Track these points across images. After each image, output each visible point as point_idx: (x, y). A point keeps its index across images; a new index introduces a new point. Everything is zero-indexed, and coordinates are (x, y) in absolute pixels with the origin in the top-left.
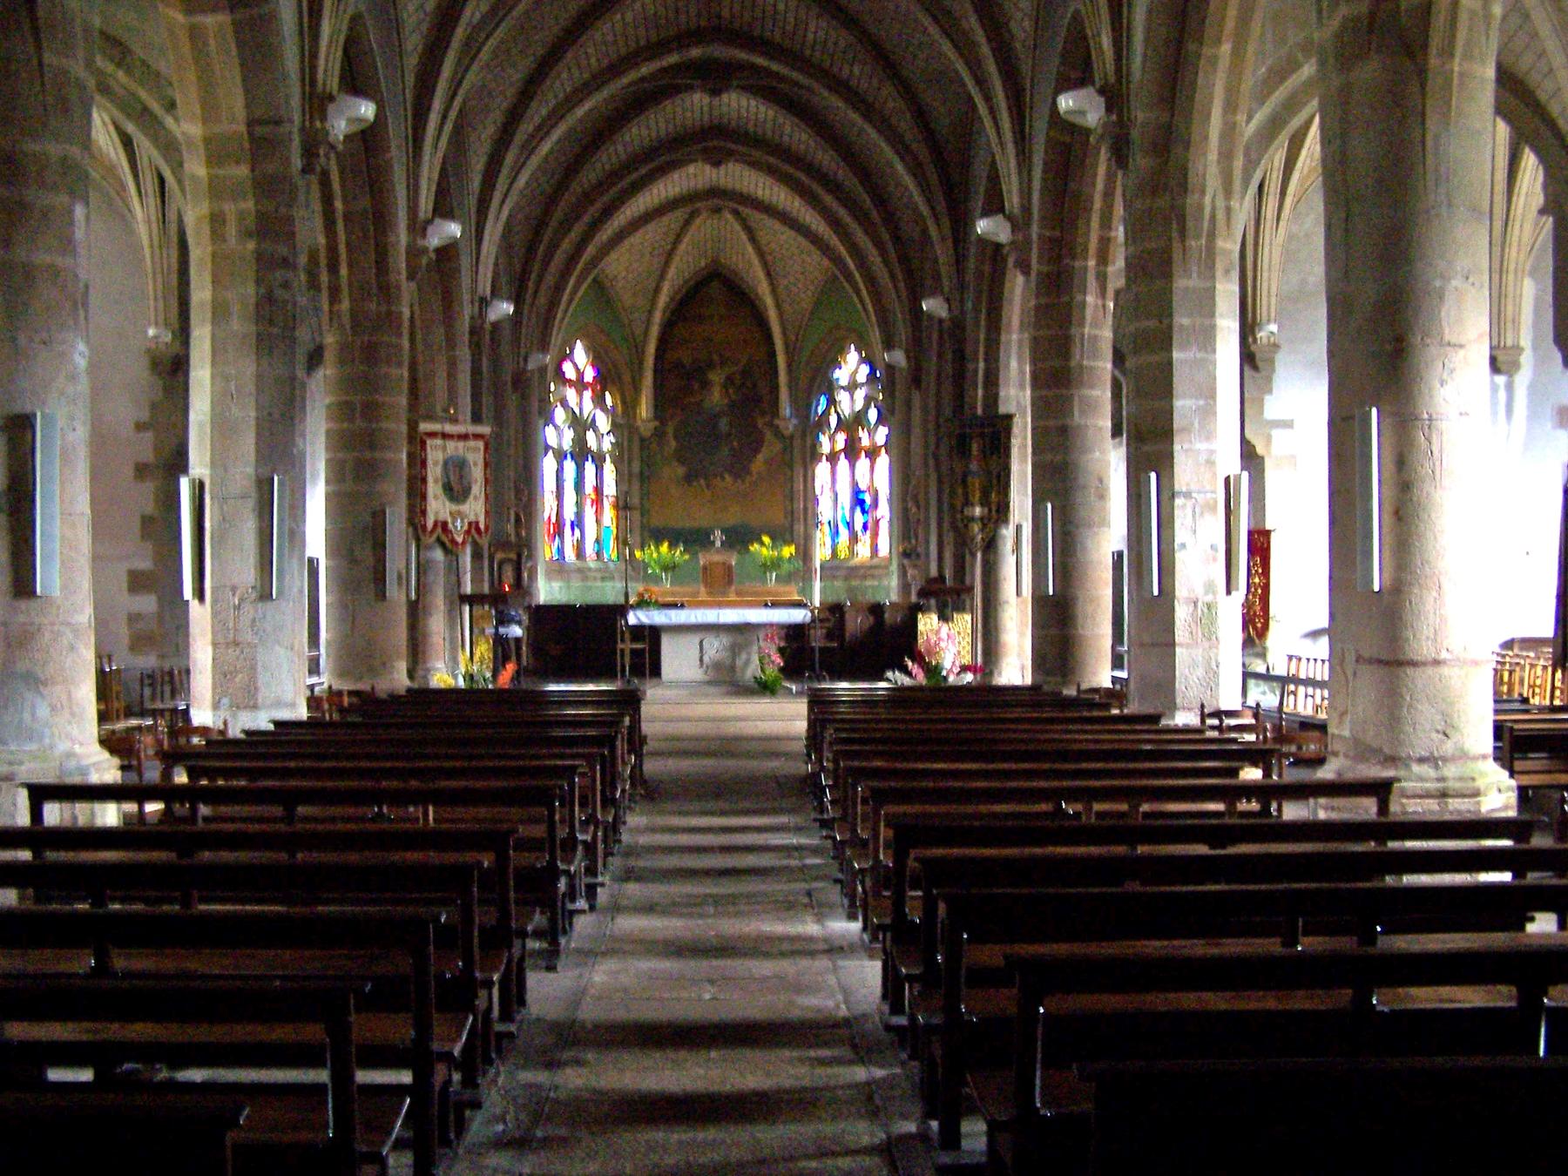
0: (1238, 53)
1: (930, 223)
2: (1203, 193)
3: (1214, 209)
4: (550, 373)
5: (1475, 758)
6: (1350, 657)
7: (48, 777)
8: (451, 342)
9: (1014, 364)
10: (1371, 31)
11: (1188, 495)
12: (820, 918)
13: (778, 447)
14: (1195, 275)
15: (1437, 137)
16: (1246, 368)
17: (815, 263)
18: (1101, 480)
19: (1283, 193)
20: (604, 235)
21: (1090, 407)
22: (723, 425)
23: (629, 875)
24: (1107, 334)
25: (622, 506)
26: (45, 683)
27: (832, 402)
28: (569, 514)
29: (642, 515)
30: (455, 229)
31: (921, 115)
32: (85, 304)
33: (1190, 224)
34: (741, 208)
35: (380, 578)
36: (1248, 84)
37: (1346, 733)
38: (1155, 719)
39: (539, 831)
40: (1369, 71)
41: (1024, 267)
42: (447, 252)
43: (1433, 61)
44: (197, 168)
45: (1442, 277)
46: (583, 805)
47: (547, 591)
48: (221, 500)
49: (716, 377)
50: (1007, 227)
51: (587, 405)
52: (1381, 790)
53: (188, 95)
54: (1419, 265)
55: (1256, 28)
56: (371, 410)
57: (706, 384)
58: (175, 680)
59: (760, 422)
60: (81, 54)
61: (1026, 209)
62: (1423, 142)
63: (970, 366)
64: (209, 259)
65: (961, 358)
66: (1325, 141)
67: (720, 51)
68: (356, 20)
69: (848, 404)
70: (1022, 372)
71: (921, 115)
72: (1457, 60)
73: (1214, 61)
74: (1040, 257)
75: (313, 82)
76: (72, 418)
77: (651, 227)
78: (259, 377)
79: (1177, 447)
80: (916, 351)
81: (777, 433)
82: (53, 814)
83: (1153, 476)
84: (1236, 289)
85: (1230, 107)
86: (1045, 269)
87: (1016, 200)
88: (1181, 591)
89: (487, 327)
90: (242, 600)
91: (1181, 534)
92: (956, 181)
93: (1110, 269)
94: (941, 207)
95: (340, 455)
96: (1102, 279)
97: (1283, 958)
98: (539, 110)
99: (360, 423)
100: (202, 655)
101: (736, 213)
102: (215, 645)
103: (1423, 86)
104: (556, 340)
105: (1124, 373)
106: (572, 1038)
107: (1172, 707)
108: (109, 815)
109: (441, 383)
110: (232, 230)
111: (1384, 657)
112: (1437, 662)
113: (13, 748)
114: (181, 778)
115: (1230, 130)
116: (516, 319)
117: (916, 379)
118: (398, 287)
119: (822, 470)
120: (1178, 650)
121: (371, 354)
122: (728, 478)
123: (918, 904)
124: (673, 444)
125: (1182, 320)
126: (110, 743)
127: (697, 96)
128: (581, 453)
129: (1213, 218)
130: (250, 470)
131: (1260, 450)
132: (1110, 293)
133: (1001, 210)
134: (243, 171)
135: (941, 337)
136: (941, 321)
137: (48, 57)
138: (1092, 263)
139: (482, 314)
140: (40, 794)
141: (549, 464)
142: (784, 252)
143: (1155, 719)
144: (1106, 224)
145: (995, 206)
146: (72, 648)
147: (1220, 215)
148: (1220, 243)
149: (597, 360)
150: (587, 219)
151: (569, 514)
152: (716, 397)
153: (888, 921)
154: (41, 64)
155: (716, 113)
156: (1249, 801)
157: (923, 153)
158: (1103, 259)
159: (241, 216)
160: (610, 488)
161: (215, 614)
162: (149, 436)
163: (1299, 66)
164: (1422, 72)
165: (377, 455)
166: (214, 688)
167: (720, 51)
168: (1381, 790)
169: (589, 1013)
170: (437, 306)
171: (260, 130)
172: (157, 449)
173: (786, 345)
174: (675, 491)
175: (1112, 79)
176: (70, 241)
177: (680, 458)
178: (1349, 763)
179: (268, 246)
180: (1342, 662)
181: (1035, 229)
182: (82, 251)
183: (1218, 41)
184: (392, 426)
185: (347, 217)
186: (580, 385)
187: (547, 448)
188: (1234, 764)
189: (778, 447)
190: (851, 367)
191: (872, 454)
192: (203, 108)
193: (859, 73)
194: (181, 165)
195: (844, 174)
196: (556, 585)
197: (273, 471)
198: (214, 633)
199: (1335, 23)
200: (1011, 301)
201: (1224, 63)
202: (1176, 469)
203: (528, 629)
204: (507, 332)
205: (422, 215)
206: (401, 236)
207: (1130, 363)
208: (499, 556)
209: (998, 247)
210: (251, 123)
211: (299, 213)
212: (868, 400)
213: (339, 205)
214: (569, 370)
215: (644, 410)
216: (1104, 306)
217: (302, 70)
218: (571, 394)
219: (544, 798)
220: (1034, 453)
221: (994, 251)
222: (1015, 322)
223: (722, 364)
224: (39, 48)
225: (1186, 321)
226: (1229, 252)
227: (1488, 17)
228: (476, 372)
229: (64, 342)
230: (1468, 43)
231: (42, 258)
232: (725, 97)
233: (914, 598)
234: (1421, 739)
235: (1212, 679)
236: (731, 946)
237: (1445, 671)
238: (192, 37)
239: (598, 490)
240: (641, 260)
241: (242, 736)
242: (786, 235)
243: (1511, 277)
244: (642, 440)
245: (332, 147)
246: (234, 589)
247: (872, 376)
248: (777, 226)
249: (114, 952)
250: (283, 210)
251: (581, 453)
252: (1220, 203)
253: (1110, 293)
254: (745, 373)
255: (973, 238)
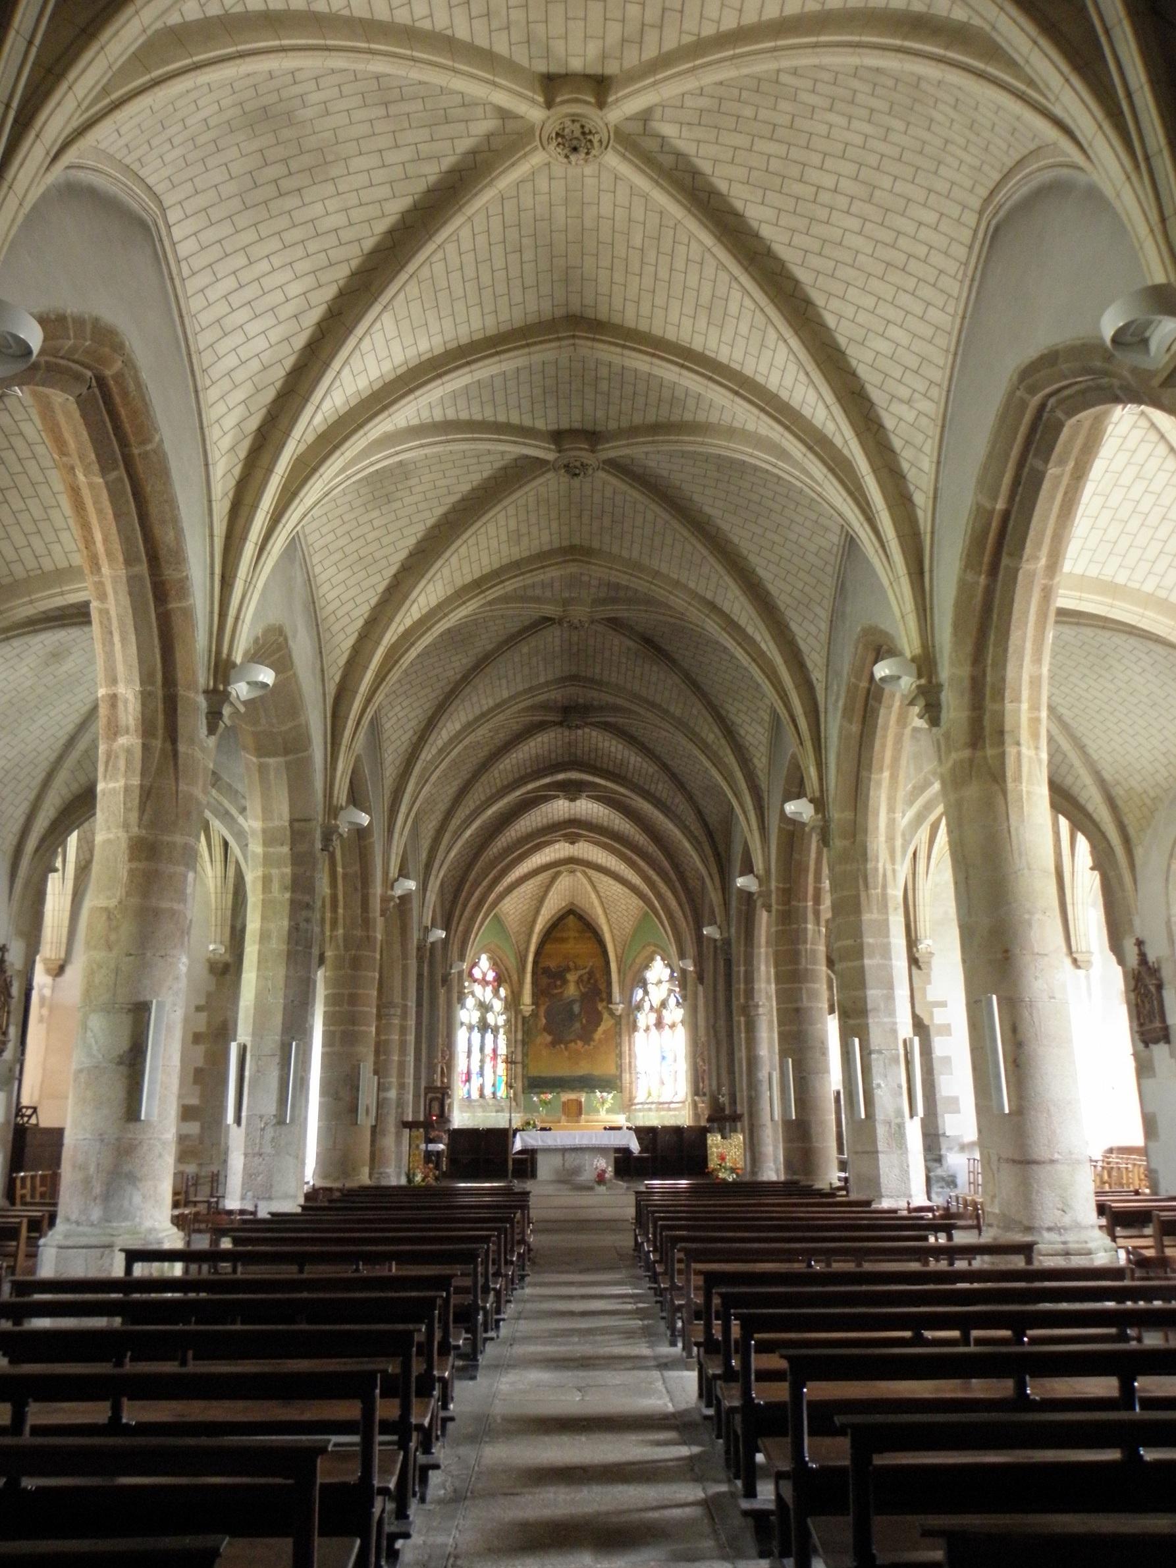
0: (894, 777)
1: (708, 881)
2: (877, 861)
3: (885, 870)
4: (465, 975)
5: (1086, 1228)
6: (994, 1158)
7: (136, 1245)
8: (405, 956)
9: (763, 968)
10: (971, 766)
11: (880, 1052)
12: (652, 1345)
13: (612, 1022)
14: (875, 911)
15: (1017, 829)
16: (914, 968)
17: (635, 901)
18: (823, 1043)
19: (929, 857)
20: (500, 888)
21: (814, 995)
22: (576, 1008)
23: (519, 1316)
24: (822, 949)
25: (509, 1061)
26: (140, 1180)
27: (646, 993)
28: (475, 1068)
29: (523, 1068)
30: (411, 885)
31: (700, 813)
32: (188, 933)
33: (870, 880)
34: (587, 870)
35: (353, 1109)
36: (901, 794)
37: (997, 1211)
38: (868, 1203)
39: (467, 1282)
40: (972, 791)
41: (769, 909)
42: (405, 899)
43: (1010, 785)
44: (256, 847)
45: (1029, 912)
46: (494, 1264)
47: (460, 1119)
48: (257, 1058)
49: (572, 977)
50: (756, 881)
51: (487, 994)
52: (1026, 1250)
53: (255, 805)
54: (1014, 905)
55: (903, 762)
56: (353, 999)
57: (565, 982)
58: (216, 1181)
59: (600, 1007)
60: (200, 783)
61: (768, 871)
62: (1009, 832)
63: (735, 969)
64: (260, 905)
65: (728, 963)
66: (950, 832)
67: (574, 775)
68: (358, 759)
69: (657, 994)
70: (768, 972)
71: (700, 813)
72: (1024, 784)
73: (879, 783)
74: (777, 901)
75: (331, 796)
76: (175, 1005)
77: (531, 881)
78: (287, 977)
79: (870, 1021)
80: (699, 962)
81: (611, 1013)
82: (140, 1270)
83: (857, 1040)
84: (902, 919)
85: (891, 809)
86: (780, 907)
87: (761, 866)
88: (880, 1116)
89: (428, 946)
90: (266, 1124)
91: (877, 1080)
92: (721, 851)
93: (822, 907)
94: (714, 870)
95: (332, 1028)
96: (817, 914)
97: (947, 1272)
98: (462, 813)
99: (346, 1007)
100: (236, 1163)
101: (585, 873)
102: (246, 1155)
103: (1006, 799)
104: (470, 953)
105: (833, 971)
106: (486, 1429)
107: (880, 1196)
108: (177, 1270)
109: (397, 983)
110: (276, 886)
111: (1016, 1157)
112: (1052, 1161)
113: (115, 1224)
114: (226, 1244)
115: (892, 823)
116: (445, 942)
117: (700, 978)
118: (375, 919)
119: (639, 1036)
120: (881, 1156)
121: (356, 964)
122: (580, 1043)
123: (719, 1328)
124: (544, 1021)
125: (869, 940)
126: (178, 1221)
127: (561, 802)
128: (484, 1026)
129: (885, 875)
130: (278, 1038)
131: (926, 1022)
132: (823, 923)
133: (751, 871)
134: (286, 849)
135: (715, 952)
136: (716, 940)
137: (182, 787)
138: (810, 904)
139: (425, 940)
140: (133, 1256)
141: (461, 1036)
142: (613, 897)
143: (868, 1203)
144: (818, 879)
145: (748, 869)
146: (160, 1156)
147: (889, 874)
148: (890, 891)
149: (495, 964)
150: (491, 876)
151: (475, 1068)
152: (572, 990)
153: (701, 1340)
154: (177, 791)
155: (572, 812)
156: (937, 1260)
157: (703, 838)
158: (817, 900)
159: (283, 876)
160: (503, 1050)
161: (247, 1135)
162: (204, 1015)
163: (931, 784)
164: (1004, 792)
165: (356, 1028)
166: (243, 1184)
167: (574, 775)
168: (1026, 1250)
169: (499, 1409)
170: (396, 932)
171: (296, 825)
172: (209, 1024)
173: (617, 957)
174: (544, 1052)
175: (817, 794)
176: (183, 892)
177: (548, 1029)
178: (1000, 1231)
179: (299, 897)
180: (989, 1163)
181: (773, 885)
182: (190, 900)
183: (881, 770)
184: (366, 1009)
185: (345, 875)
186: (484, 982)
187: (462, 1024)
188: (922, 1233)
189: (612, 1022)
190: (658, 971)
191: (672, 1026)
192: (263, 812)
193: (663, 788)
194: (247, 845)
195: (652, 848)
196: (466, 1115)
197: (293, 1038)
198: (246, 1147)
199: (950, 763)
200: (760, 929)
201: (885, 783)
202: (871, 1035)
203: (448, 1145)
204: (439, 946)
205: (391, 875)
206: (378, 890)
207: (837, 967)
208: (430, 1095)
209: (750, 894)
210: (292, 821)
211: (318, 876)
212: (671, 991)
213: (340, 870)
214: (477, 973)
215: (527, 997)
216: (819, 931)
217: (325, 789)
218: (477, 989)
219: (469, 1258)
220: (779, 1026)
221: (747, 897)
222: (763, 940)
223: (576, 968)
224: (177, 779)
225: (871, 940)
226: (895, 896)
227: (1040, 761)
228: (420, 976)
229: (174, 956)
230: (1030, 773)
231: (165, 905)
232: (578, 802)
233: (703, 1123)
234: (1048, 1214)
235: (905, 1186)
236: (580, 1380)
237: (1059, 1167)
238: (260, 772)
239: (495, 1051)
240: (522, 904)
241: (269, 1216)
242: (618, 888)
243: (1080, 907)
244: (524, 1018)
245: (341, 835)
246: (261, 1117)
247: (672, 976)
248: (611, 882)
249: (125, 1402)
250: (308, 874)
251: (484, 1026)
252: (889, 867)
253: (823, 923)
254: (591, 974)
255: (734, 891)
